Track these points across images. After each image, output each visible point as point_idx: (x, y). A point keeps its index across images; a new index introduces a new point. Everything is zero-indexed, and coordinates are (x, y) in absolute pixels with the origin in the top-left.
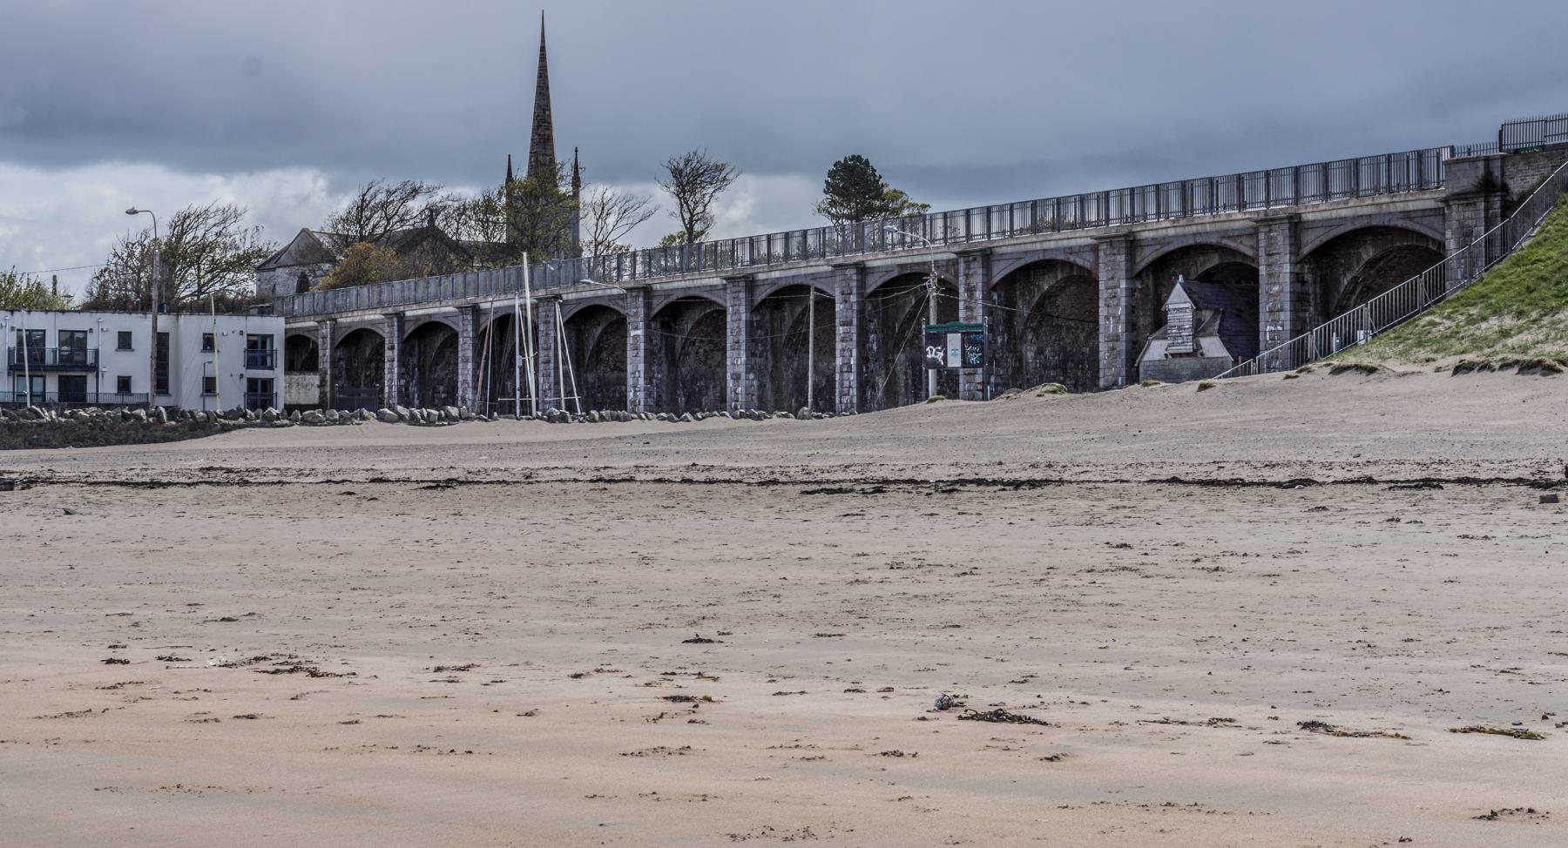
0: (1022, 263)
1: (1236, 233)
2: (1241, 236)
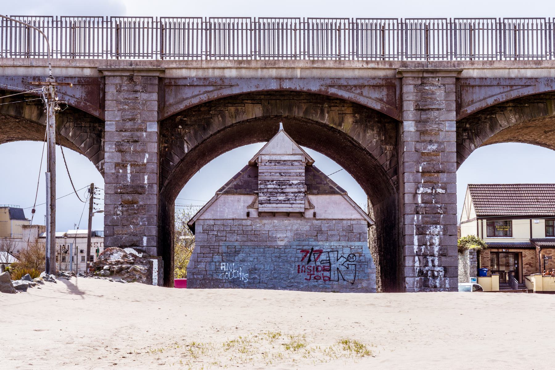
0: (514, 94)
1: (352, 83)
2: (362, 86)
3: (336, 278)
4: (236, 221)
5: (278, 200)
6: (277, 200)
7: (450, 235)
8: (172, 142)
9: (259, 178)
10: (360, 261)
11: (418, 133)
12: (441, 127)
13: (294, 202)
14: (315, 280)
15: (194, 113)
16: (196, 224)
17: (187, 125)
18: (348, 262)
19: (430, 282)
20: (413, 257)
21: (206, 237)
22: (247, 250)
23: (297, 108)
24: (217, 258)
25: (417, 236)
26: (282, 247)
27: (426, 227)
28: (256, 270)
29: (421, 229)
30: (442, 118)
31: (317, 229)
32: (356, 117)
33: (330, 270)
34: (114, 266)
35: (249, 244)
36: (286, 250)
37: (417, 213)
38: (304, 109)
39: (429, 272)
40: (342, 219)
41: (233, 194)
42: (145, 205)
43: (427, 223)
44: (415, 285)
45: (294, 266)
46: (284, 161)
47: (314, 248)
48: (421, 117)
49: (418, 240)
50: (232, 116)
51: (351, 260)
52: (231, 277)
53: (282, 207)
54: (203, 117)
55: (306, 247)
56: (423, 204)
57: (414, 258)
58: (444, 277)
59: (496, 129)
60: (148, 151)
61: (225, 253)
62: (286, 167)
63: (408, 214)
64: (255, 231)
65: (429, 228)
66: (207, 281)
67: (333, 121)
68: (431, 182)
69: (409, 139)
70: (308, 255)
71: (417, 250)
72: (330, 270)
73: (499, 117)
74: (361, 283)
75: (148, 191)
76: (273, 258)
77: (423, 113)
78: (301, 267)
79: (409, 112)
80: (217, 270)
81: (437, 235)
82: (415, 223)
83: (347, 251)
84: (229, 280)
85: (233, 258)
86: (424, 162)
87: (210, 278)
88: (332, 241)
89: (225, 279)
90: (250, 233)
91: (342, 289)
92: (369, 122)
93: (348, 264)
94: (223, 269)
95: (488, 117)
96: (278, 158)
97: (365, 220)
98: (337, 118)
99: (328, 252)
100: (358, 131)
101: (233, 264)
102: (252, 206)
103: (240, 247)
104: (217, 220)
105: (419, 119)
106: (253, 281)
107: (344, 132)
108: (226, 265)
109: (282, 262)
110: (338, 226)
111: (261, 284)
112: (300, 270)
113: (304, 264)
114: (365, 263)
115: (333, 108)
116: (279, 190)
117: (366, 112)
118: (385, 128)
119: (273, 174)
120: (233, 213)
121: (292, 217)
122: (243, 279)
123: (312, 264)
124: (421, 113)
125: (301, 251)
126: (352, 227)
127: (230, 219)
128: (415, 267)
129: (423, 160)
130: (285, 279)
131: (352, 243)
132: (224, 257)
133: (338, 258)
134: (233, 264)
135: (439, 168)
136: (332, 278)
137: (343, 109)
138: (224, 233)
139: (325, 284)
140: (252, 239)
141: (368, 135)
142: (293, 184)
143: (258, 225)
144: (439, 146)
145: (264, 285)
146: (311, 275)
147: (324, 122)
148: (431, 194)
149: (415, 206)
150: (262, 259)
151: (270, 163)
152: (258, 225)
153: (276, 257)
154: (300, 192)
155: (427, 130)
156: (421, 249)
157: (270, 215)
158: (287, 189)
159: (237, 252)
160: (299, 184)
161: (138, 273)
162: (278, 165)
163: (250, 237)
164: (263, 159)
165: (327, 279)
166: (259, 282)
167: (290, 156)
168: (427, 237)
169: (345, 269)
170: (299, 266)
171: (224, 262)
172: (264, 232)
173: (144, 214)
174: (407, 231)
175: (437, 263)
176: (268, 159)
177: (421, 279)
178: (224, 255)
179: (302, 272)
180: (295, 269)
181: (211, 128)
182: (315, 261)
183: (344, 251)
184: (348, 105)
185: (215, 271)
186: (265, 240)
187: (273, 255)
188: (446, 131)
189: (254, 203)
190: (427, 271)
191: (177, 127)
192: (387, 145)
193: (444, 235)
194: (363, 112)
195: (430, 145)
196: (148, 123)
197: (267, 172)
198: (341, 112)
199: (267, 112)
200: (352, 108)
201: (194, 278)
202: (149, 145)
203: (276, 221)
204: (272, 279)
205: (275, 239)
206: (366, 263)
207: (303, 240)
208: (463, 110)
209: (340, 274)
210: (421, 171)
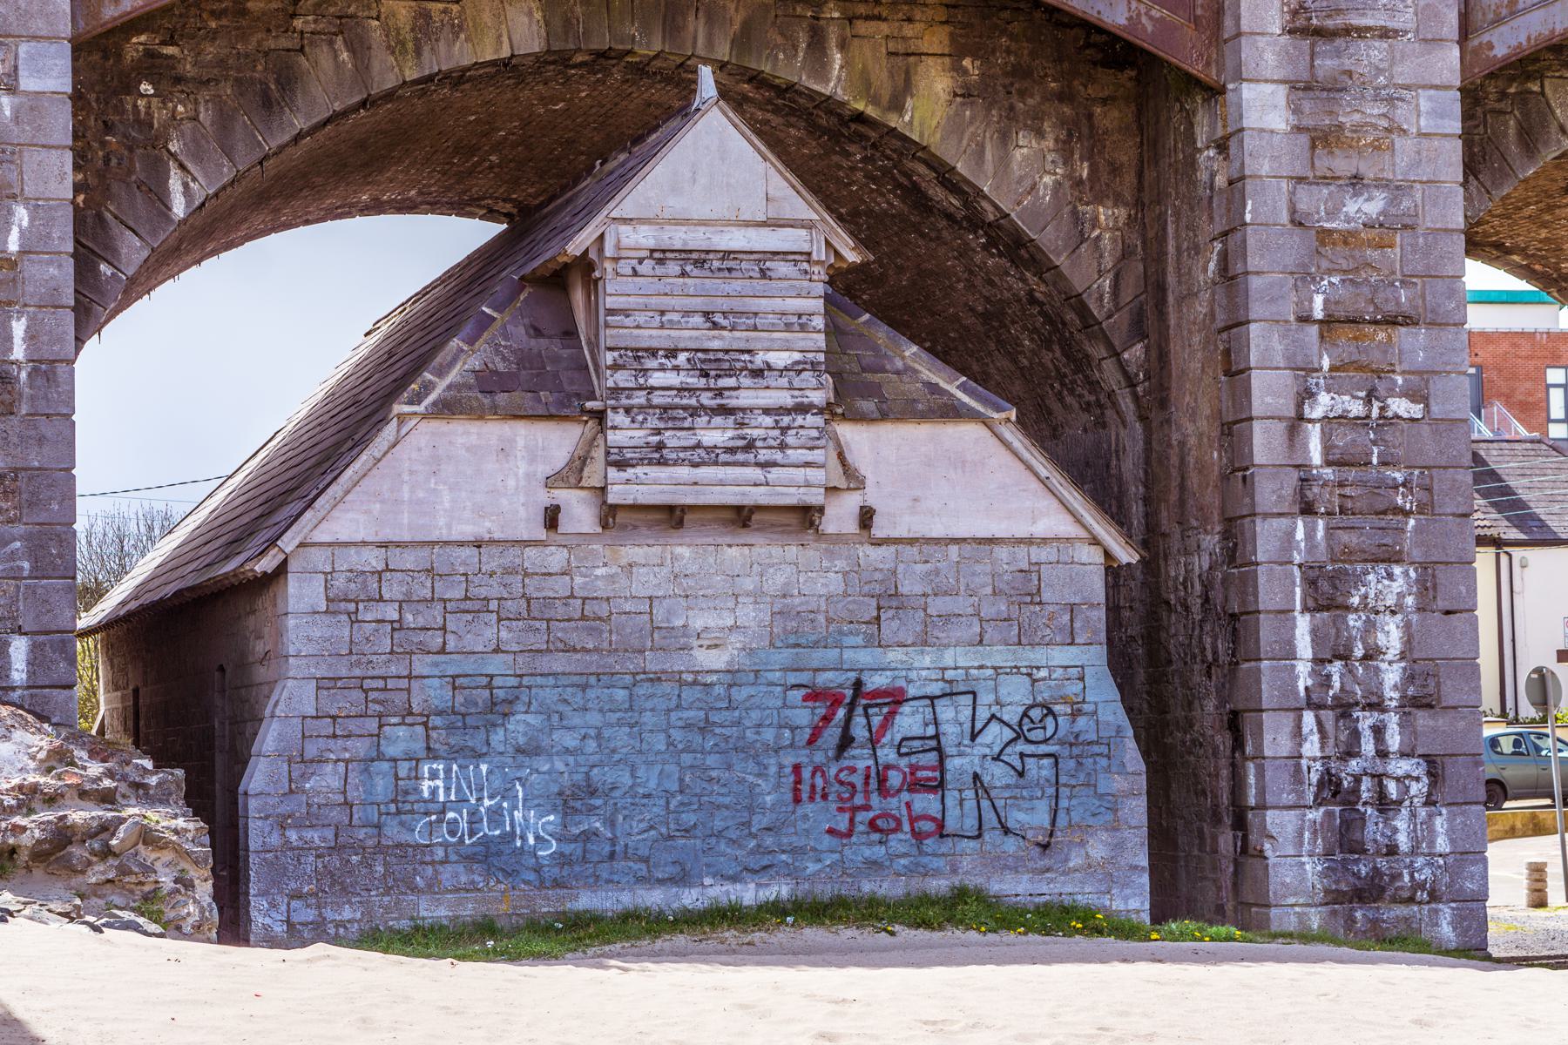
3: (970, 824)
4: (495, 550)
5: (698, 446)
6: (693, 448)
7: (1448, 613)
8: (107, 160)
9: (608, 337)
10: (1075, 741)
11: (1304, 139)
12: (1402, 112)
13: (778, 456)
14: (876, 837)
15: (214, 25)
16: (293, 566)
17: (178, 80)
18: (1021, 747)
19: (1370, 827)
20: (1291, 715)
21: (346, 633)
22: (549, 695)
23: (702, 21)
24: (401, 739)
25: (1308, 617)
26: (714, 678)
27: (1346, 573)
28: (593, 793)
29: (1324, 586)
30: (1404, 72)
31: (878, 589)
32: (965, 72)
33: (939, 786)
34: (18, 820)
35: (558, 663)
36: (734, 690)
37: (1308, 509)
38: (737, 27)
39: (1366, 783)
40: (992, 541)
41: (479, 414)
42: (16, 470)
43: (1349, 554)
44: (1306, 847)
45: (773, 770)
46: (727, 254)
47: (865, 677)
48: (1312, 66)
49: (1314, 632)
50: (403, 43)
51: (1037, 735)
52: (472, 834)
53: (722, 484)
54: (259, 43)
55: (830, 675)
56: (1329, 470)
57: (1299, 720)
58: (1426, 804)
59: (1546, 144)
60: (29, 190)
61: (440, 713)
62: (736, 285)
63: (1266, 516)
64: (584, 599)
65: (1359, 580)
66: (355, 858)
67: (866, 87)
68: (1361, 368)
69: (1265, 168)
70: (841, 713)
71: (1310, 682)
72: (939, 786)
73: (1555, 90)
74: (1083, 844)
75: (32, 398)
76: (677, 735)
77: (1322, 46)
78: (806, 774)
79: (1261, 42)
80: (403, 799)
81: (1393, 613)
82: (1297, 559)
83: (1016, 693)
84: (462, 850)
85: (482, 735)
86: (1330, 272)
87: (370, 843)
88: (947, 646)
89: (445, 845)
90: (561, 611)
91: (996, 877)
92: (1023, 94)
93: (1022, 755)
94: (434, 791)
95: (1512, 90)
96: (695, 238)
97: (1095, 541)
98: (884, 75)
99: (932, 698)
100: (974, 135)
101: (484, 768)
102: (572, 473)
103: (513, 681)
104: (398, 545)
105: (1306, 76)
106: (579, 852)
107: (915, 137)
108: (448, 771)
109: (716, 749)
110: (974, 574)
111: (620, 865)
112: (805, 788)
113: (819, 758)
114: (1096, 749)
115: (862, 27)
116: (706, 399)
117: (1008, 52)
118: (1091, 127)
119: (675, 317)
120: (480, 512)
121: (763, 528)
122: (531, 841)
123: (860, 759)
124: (1313, 46)
125: (806, 698)
126: (1034, 576)
127: (461, 544)
128: (1304, 762)
129: (1325, 264)
130: (733, 834)
131: (1038, 656)
132: (434, 734)
133: (978, 726)
134: (484, 768)
135: (1398, 303)
136: (951, 825)
137: (908, 30)
138: (435, 615)
139: (921, 853)
140: (574, 639)
141: (1018, 154)
142: (770, 368)
143: (599, 572)
144: (1393, 201)
145: (636, 866)
146: (855, 810)
147: (827, 89)
148: (1363, 422)
149: (1295, 475)
150: (621, 738)
151: (661, 261)
152: (599, 572)
153: (688, 727)
154: (802, 409)
155: (1341, 127)
156: (1329, 676)
157: (659, 523)
158: (742, 393)
159: (498, 709)
160: (796, 369)
161: (167, 856)
162: (696, 272)
163: (564, 630)
164: (625, 242)
165: (927, 826)
166: (612, 856)
167: (752, 232)
168: (1353, 620)
169: (1011, 778)
170: (797, 769)
171: (436, 758)
172: (628, 607)
173: (10, 521)
174: (1268, 595)
175: (1398, 738)
176: (651, 243)
177: (1329, 814)
178: (436, 721)
179: (812, 799)
180: (778, 786)
181: (300, 101)
182: (874, 742)
183: (1003, 691)
184: (930, 12)
185: (393, 808)
186: (636, 643)
187: (674, 716)
188: (1421, 135)
189: (578, 464)
190: (1357, 780)
191: (130, 88)
192: (1101, 203)
193: (1420, 609)
194: (993, 52)
195: (1356, 195)
196: (24, 49)
197: (646, 309)
198: (901, 48)
199: (566, 33)
200: (948, 29)
201: (288, 842)
202: (32, 158)
203: (684, 551)
204: (670, 838)
205: (679, 639)
206: (1103, 749)
207: (815, 645)
208: (1476, 43)
209: (985, 803)
210: (1318, 314)
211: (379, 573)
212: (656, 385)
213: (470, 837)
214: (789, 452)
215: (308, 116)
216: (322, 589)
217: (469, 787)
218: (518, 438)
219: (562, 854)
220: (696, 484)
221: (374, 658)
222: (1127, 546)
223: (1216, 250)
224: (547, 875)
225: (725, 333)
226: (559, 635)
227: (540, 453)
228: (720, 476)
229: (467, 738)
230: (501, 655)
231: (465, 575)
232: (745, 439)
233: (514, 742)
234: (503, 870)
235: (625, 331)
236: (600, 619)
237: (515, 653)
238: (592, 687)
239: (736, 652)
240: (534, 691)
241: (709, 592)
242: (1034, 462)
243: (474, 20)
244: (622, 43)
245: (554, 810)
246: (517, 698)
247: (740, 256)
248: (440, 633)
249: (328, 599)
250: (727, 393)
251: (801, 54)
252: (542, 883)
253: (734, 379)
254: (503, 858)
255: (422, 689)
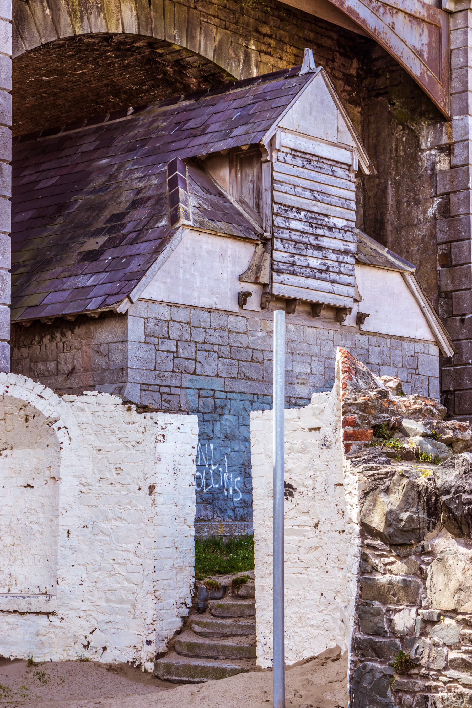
5: (308, 266)
23: (203, 36)
52: (207, 486)
101: (212, 446)
103: (223, 395)
104: (177, 305)
116: (311, 239)
127: (203, 309)
134: (212, 446)
140: (249, 373)
154: (346, 252)
158: (324, 238)
167: (331, 148)
199: (147, 26)
211: (168, 321)
212: (293, 228)
213: (206, 487)
214: (341, 276)
215: (31, 44)
216: (143, 328)
217: (206, 458)
218: (228, 249)
219: (244, 501)
220: (308, 288)
221: (165, 374)
222: (450, 348)
223: (435, 203)
224: (238, 513)
225: (319, 204)
226: (243, 369)
227: (237, 260)
228: (317, 285)
229: (205, 427)
230: (219, 378)
231: (204, 328)
232: (325, 265)
233: (225, 432)
234: (220, 509)
235: (281, 194)
236: (258, 362)
237: (225, 378)
238: (255, 402)
239: (311, 388)
240: (232, 401)
241: (301, 352)
242: (419, 297)
243: (107, 7)
244: (170, 39)
245: (240, 474)
246: (226, 405)
247: (325, 161)
248: (194, 362)
249: (146, 335)
250: (319, 238)
251: (241, 65)
252: (236, 517)
253: (322, 230)
254: (221, 502)
255: (186, 395)
